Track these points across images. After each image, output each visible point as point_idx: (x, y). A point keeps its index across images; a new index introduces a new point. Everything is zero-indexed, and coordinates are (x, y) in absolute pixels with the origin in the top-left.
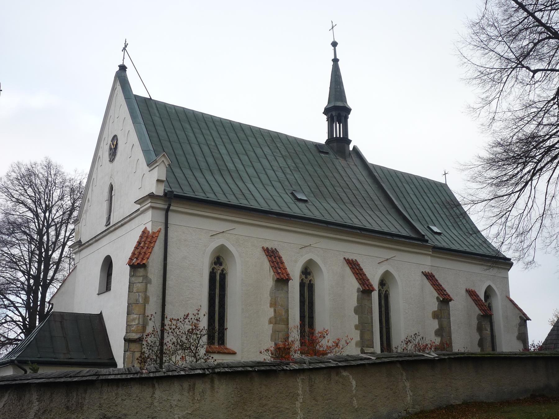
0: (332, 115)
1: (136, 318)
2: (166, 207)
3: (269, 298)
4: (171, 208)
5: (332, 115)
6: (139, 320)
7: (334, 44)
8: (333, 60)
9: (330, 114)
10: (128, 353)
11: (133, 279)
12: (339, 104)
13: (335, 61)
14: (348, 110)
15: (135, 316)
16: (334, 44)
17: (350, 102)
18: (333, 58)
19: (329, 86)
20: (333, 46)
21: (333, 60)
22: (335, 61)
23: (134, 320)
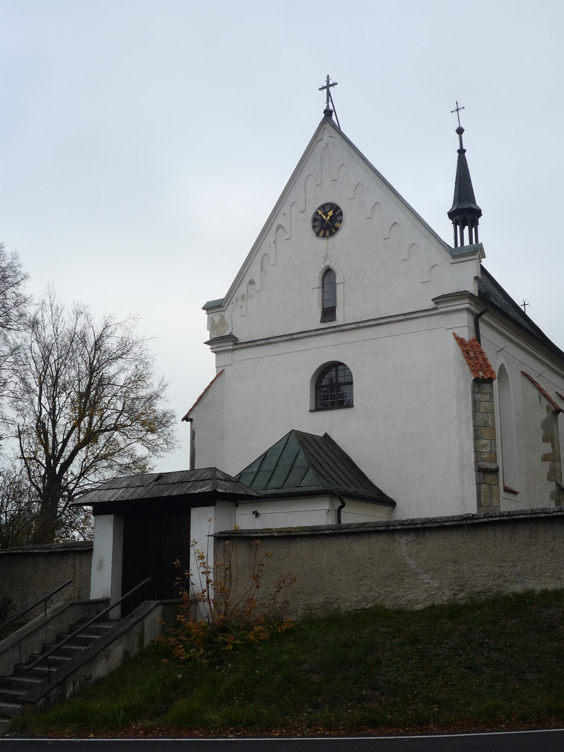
0: (456, 220)
1: (487, 444)
2: (478, 312)
3: (542, 432)
4: (483, 316)
5: (456, 220)
6: (491, 447)
7: (460, 131)
8: (458, 151)
9: (454, 219)
10: (483, 486)
11: (478, 396)
12: (465, 206)
13: (462, 152)
14: (478, 213)
15: (486, 442)
16: (460, 131)
17: (480, 202)
18: (459, 148)
19: (454, 182)
20: (458, 134)
21: (458, 151)
22: (462, 152)
23: (485, 446)
